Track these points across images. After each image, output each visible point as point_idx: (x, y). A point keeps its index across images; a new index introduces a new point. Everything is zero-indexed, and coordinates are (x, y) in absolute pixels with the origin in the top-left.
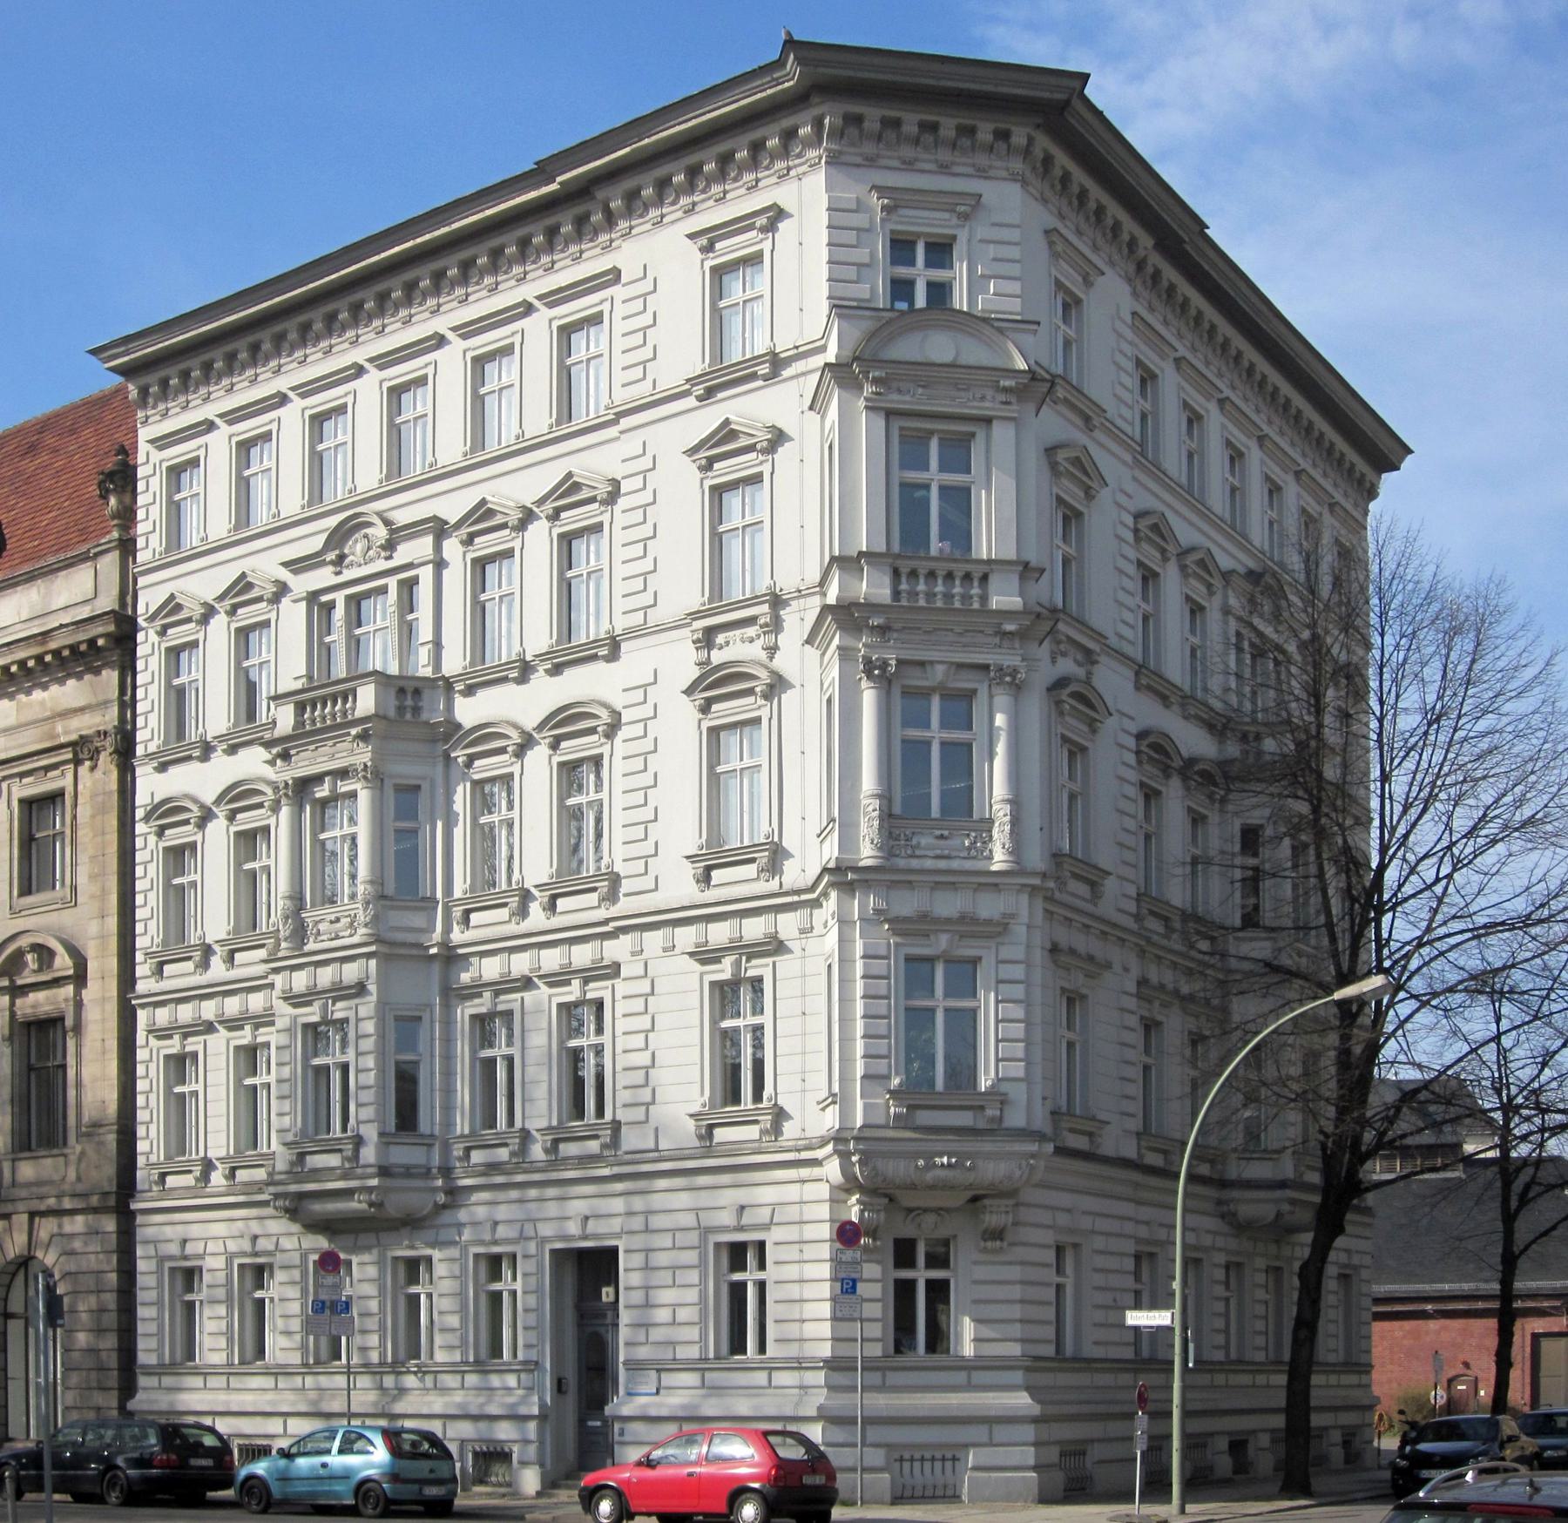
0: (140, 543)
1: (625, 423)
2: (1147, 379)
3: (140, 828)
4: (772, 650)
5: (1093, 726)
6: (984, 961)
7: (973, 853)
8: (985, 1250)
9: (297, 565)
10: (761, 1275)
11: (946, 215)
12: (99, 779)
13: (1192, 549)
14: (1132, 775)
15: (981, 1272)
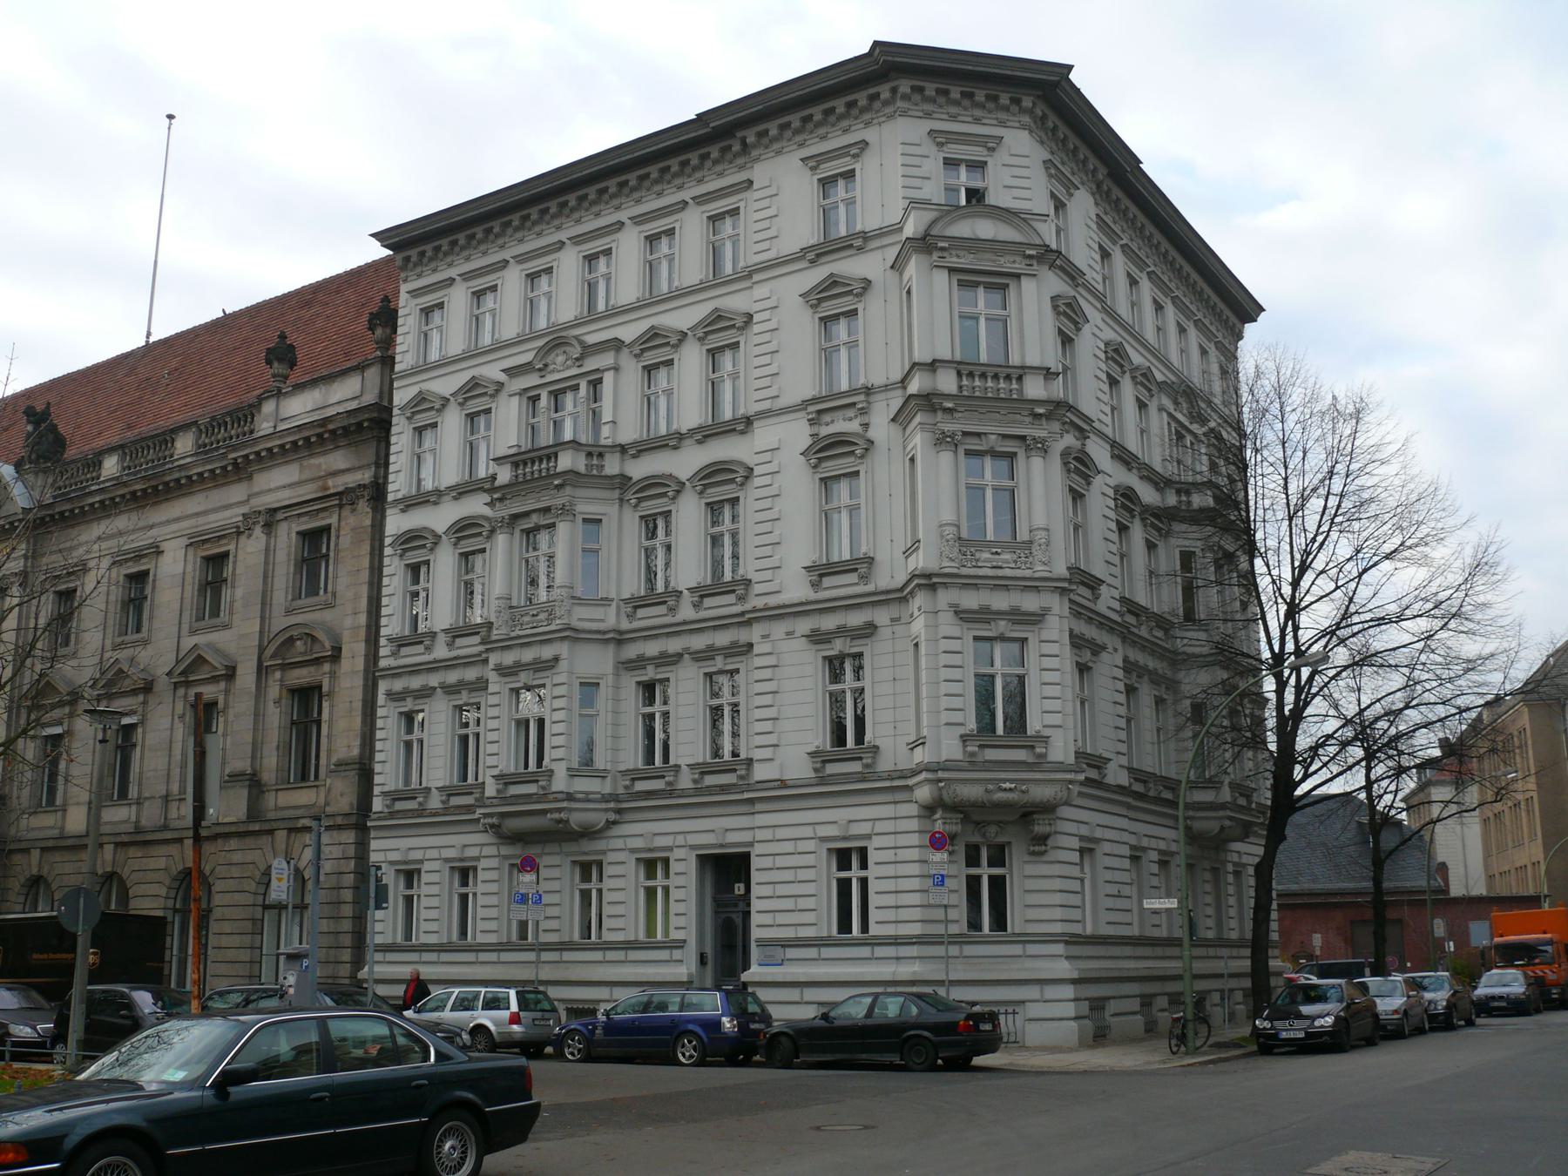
0: (398, 358)
1: (756, 278)
2: (1105, 255)
3: (388, 551)
4: (866, 426)
5: (1087, 479)
6: (1030, 641)
7: (1019, 564)
8: (1033, 853)
9: (512, 372)
10: (863, 873)
11: (980, 149)
12: (363, 515)
13: (1137, 368)
14: (1112, 515)
15: (1031, 869)
